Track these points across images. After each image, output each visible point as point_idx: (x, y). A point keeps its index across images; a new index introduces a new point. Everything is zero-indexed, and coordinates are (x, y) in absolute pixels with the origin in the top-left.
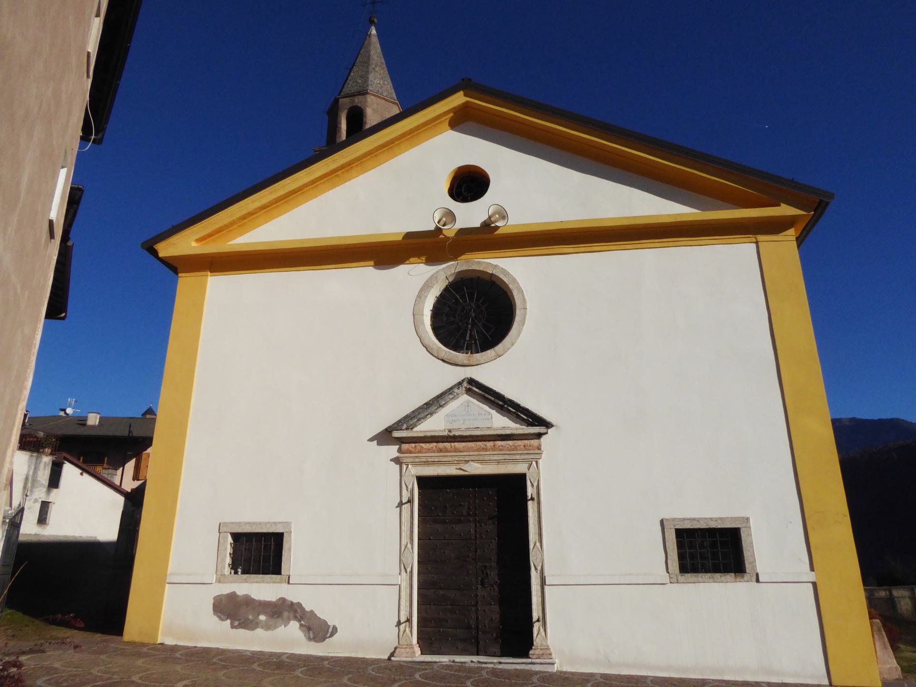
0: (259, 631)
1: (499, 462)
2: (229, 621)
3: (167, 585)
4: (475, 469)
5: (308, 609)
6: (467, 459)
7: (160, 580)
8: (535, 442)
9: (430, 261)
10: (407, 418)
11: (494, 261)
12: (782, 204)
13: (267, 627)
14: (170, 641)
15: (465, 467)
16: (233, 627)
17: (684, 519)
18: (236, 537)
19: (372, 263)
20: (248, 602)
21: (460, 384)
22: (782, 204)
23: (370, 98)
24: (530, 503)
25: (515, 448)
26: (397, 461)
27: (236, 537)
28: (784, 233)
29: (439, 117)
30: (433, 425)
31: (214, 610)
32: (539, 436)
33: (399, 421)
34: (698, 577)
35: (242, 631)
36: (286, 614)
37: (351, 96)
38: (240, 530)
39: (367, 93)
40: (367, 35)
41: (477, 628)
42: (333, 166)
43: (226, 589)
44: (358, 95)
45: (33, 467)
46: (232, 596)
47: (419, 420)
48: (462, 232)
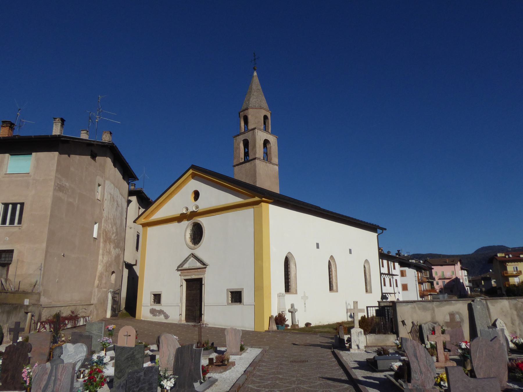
1: (198, 275)
2: (152, 315)
3: (142, 307)
4: (194, 277)
5: (165, 312)
6: (192, 274)
7: (141, 306)
8: (204, 269)
9: (188, 220)
10: (181, 264)
12: (256, 197)
13: (159, 316)
14: (143, 319)
15: (192, 276)
16: (153, 316)
17: (231, 289)
18: (232, 292)
19: (177, 222)
21: (190, 255)
22: (256, 197)
23: (250, 111)
24: (203, 285)
26: (180, 275)
27: (232, 292)
28: (259, 205)
29: (188, 177)
30: (186, 266)
31: (150, 312)
32: (205, 268)
33: (179, 265)
35: (154, 317)
36: (161, 313)
37: (243, 111)
38: (232, 291)
39: (248, 109)
40: (252, 76)
41: (195, 316)
42: (167, 195)
43: (152, 307)
44: (246, 110)
46: (153, 309)
47: (183, 264)
48: (191, 212)
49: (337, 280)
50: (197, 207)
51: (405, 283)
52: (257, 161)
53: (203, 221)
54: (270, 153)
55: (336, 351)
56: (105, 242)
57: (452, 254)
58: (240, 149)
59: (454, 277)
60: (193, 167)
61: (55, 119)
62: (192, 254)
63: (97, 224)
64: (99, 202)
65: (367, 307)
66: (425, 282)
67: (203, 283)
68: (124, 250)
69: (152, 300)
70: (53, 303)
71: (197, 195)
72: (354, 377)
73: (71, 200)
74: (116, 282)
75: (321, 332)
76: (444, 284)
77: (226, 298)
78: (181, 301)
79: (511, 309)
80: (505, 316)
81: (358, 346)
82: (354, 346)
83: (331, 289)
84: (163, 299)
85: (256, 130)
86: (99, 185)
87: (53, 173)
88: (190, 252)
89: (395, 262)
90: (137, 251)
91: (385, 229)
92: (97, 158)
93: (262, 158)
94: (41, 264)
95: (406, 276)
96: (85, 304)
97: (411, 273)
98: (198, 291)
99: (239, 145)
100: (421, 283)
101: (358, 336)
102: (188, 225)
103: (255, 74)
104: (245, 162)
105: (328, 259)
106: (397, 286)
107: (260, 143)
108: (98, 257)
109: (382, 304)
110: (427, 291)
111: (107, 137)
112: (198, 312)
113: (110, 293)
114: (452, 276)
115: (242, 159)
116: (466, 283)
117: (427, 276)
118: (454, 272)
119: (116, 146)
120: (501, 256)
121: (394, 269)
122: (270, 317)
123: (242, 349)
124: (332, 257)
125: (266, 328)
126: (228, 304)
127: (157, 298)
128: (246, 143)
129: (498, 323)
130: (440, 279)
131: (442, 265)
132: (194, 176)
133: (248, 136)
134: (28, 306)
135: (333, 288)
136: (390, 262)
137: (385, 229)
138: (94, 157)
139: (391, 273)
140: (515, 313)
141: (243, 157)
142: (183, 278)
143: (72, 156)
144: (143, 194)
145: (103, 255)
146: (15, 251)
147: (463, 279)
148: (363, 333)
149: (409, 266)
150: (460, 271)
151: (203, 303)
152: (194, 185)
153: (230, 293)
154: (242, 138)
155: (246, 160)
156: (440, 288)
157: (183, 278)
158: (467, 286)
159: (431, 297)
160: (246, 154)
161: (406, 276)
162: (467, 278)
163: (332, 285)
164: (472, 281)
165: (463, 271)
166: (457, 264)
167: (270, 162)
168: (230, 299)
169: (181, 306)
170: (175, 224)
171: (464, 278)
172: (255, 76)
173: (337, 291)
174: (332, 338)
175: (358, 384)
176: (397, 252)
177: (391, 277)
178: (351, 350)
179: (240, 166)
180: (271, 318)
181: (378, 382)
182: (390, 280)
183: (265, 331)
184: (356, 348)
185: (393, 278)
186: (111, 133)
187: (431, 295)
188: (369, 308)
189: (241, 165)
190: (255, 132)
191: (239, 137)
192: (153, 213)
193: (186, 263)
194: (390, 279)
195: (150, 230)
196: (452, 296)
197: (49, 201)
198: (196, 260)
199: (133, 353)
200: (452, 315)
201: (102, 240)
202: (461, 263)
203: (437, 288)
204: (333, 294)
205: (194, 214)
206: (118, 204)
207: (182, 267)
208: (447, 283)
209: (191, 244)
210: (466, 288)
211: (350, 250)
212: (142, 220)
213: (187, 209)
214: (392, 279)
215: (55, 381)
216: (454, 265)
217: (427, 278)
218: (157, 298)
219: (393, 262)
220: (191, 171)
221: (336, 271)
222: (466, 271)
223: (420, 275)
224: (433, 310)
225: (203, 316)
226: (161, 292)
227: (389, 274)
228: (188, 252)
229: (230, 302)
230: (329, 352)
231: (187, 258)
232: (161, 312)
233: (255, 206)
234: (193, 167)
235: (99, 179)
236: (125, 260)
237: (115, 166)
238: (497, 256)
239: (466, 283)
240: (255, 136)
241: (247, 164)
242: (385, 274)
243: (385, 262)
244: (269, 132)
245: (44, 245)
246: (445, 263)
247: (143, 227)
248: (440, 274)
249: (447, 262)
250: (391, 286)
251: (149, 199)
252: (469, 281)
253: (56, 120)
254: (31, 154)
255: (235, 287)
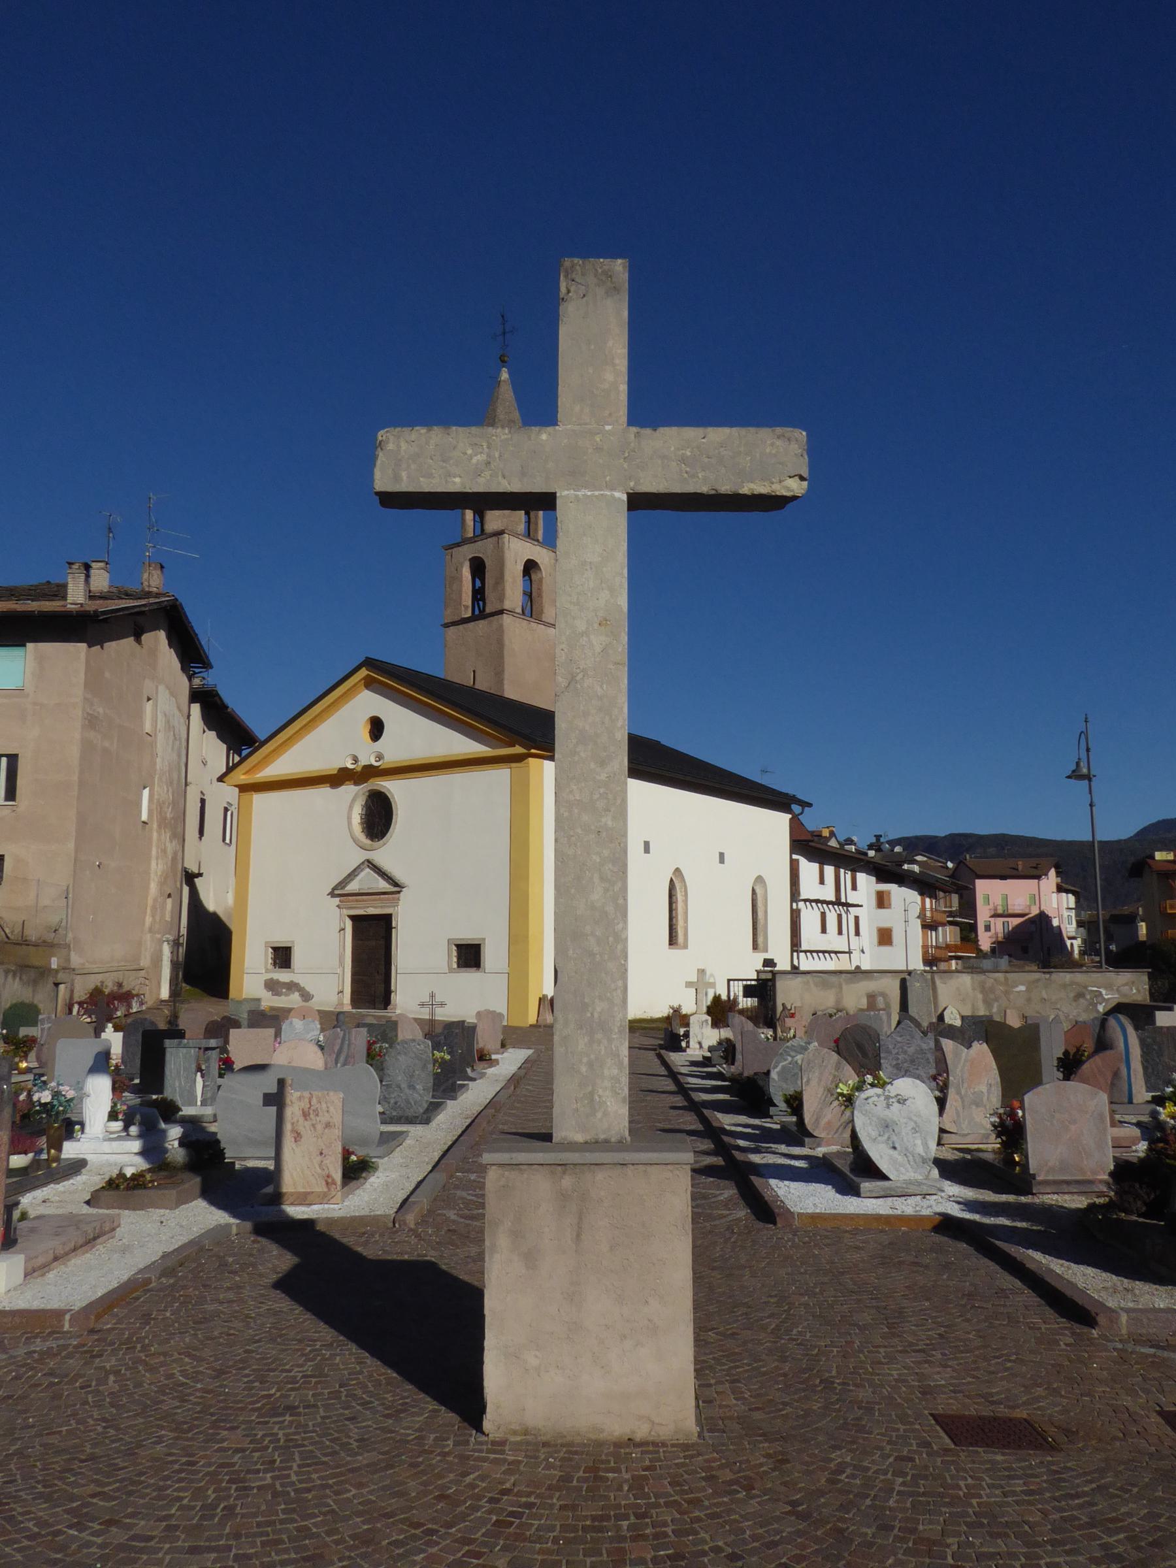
0: (283, 997)
1: (381, 907)
4: (372, 911)
8: (397, 896)
9: (356, 784)
10: (340, 883)
11: (383, 783)
13: (286, 995)
18: (458, 946)
20: (277, 982)
21: (363, 863)
25: (176, 882)
27: (458, 946)
29: (354, 685)
30: (353, 887)
32: (399, 892)
34: (883, 1085)
42: (275, 745)
45: (961, 1200)
46: (271, 980)
49: (686, 921)
50: (380, 757)
51: (885, 925)
52: (506, 619)
53: (393, 787)
54: (540, 595)
55: (663, 1052)
56: (159, 826)
57: (1069, 839)
58: (461, 581)
59: (1035, 911)
60: (369, 663)
61: (70, 564)
62: (368, 861)
63: (147, 790)
64: (149, 738)
65: (729, 981)
66: (943, 925)
67: (394, 925)
68: (184, 840)
69: (270, 961)
70: (87, 965)
71: (377, 728)
72: (715, 1124)
73: (107, 744)
74: (172, 917)
75: (645, 1028)
76: (1006, 931)
77: (444, 957)
78: (342, 963)
79: (974, 989)
80: (963, 1000)
81: (700, 1043)
82: (693, 1043)
83: (673, 940)
84: (297, 958)
85: (506, 535)
86: (149, 699)
87: (79, 692)
88: (362, 856)
89: (856, 871)
90: (200, 838)
91: (810, 805)
92: (144, 637)
93: (519, 610)
94: (68, 887)
95: (889, 907)
96: (132, 968)
97: (904, 898)
98: (382, 942)
99: (458, 570)
100: (929, 926)
101: (701, 1027)
102: (356, 794)
103: (505, 375)
104: (473, 619)
105: (669, 874)
106: (857, 933)
107: (513, 570)
108: (149, 864)
109: (763, 976)
110: (948, 947)
111: (155, 577)
112: (382, 987)
113: (166, 943)
114: (1030, 906)
115: (466, 607)
116: (1069, 927)
117: (951, 907)
118: (1035, 898)
119: (181, 604)
120: (1165, 858)
121: (854, 888)
122: (540, 999)
123: (503, 1045)
124: (677, 870)
125: (532, 1019)
126: (451, 970)
127: (282, 956)
128: (478, 567)
129: (946, 1014)
130: (996, 915)
131: (1003, 877)
132: (369, 684)
133: (482, 549)
134: (57, 971)
135: (676, 940)
136: (842, 871)
137: (810, 805)
138: (138, 637)
139: (843, 900)
140: (980, 996)
141: (469, 603)
142: (346, 912)
143: (106, 645)
144: (216, 698)
145: (157, 859)
146: (6, 858)
147: (1060, 917)
148: (710, 1022)
149: (901, 879)
150: (1055, 895)
151: (393, 967)
152: (369, 703)
153: (455, 948)
154: (468, 551)
155: (477, 612)
156: (994, 940)
157: (346, 912)
158: (1070, 938)
159: (957, 964)
160: (479, 595)
161: (889, 907)
162: (1073, 913)
163: (677, 932)
164: (1089, 922)
165: (1064, 894)
166: (1046, 875)
167: (540, 621)
168: (455, 959)
169: (341, 973)
170: (325, 791)
171: (1066, 914)
172: (504, 381)
173: (685, 947)
174: (661, 1039)
175: (752, 1178)
176: (874, 840)
177: (842, 910)
178: (688, 1050)
179: (461, 627)
180: (541, 1000)
181: (757, 1132)
182: (840, 916)
183: (531, 1025)
184: (698, 1046)
185: (847, 912)
186: (162, 567)
187: (957, 958)
188: (731, 982)
189: (465, 625)
190: (504, 543)
191: (460, 549)
192: (267, 760)
193: (352, 880)
194: (840, 916)
195: (259, 800)
196: (1022, 962)
197: (74, 752)
198: (376, 875)
199: (385, 1031)
200: (871, 998)
201: (155, 826)
202: (1058, 874)
203: (985, 942)
204: (676, 953)
205: (370, 772)
206: (174, 735)
207: (343, 888)
208: (1013, 929)
209: (362, 838)
210: (1068, 943)
211: (722, 855)
212: (240, 776)
213: (356, 760)
214: (844, 916)
215: (349, 1045)
216: (1038, 877)
217: (951, 914)
218: (282, 956)
219: (851, 871)
220: (364, 672)
221: (686, 901)
222: (1073, 894)
223: (928, 905)
224: (840, 987)
225: (393, 995)
226: (293, 942)
227: (838, 902)
228: (359, 856)
229: (455, 966)
230: (652, 1054)
231: (355, 870)
232: (292, 987)
233: (513, 765)
234: (369, 663)
235: (148, 686)
236: (186, 865)
237: (170, 646)
238: (1153, 857)
239: (1069, 927)
240: (503, 552)
241: (482, 624)
242: (828, 903)
243: (829, 870)
244: (538, 541)
245: (71, 845)
246: (1014, 873)
247: (240, 792)
248: (997, 901)
249: (1020, 868)
250: (840, 932)
251: (227, 707)
252: (1080, 924)
253: (74, 566)
254: (24, 645)
255: (468, 935)
